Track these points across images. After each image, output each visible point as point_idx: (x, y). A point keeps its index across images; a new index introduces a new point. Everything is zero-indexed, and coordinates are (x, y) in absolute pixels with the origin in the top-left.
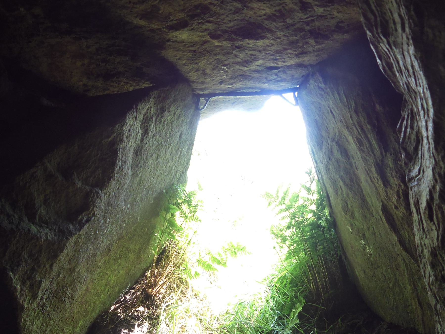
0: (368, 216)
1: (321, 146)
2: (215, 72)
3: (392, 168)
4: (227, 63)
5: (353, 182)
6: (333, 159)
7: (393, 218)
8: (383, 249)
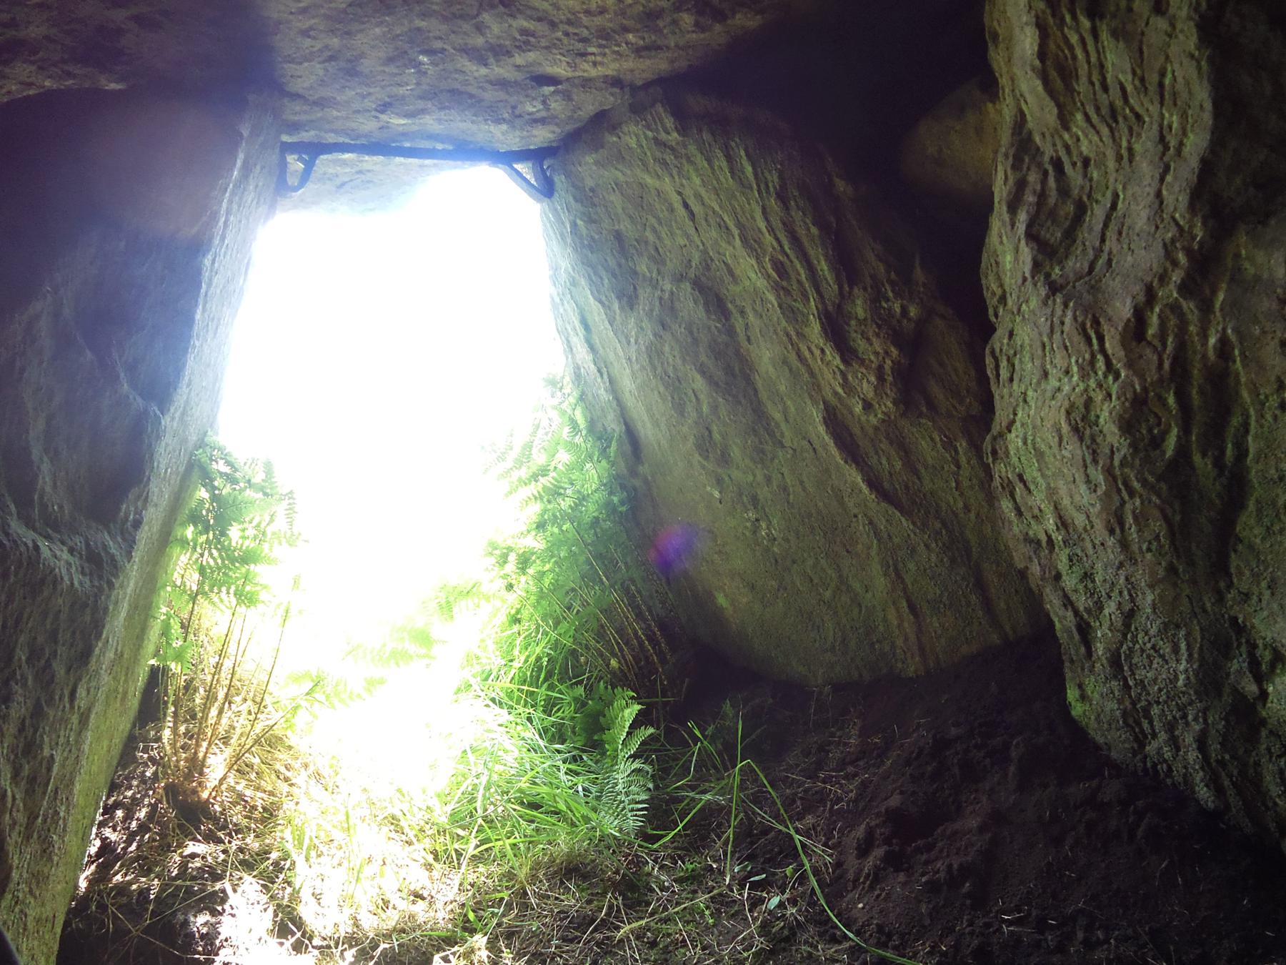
0: (768, 448)
1: (630, 298)
2: (392, 69)
3: (865, 319)
4: (438, 45)
5: (734, 376)
6: (675, 327)
7: (851, 435)
8: (810, 515)
